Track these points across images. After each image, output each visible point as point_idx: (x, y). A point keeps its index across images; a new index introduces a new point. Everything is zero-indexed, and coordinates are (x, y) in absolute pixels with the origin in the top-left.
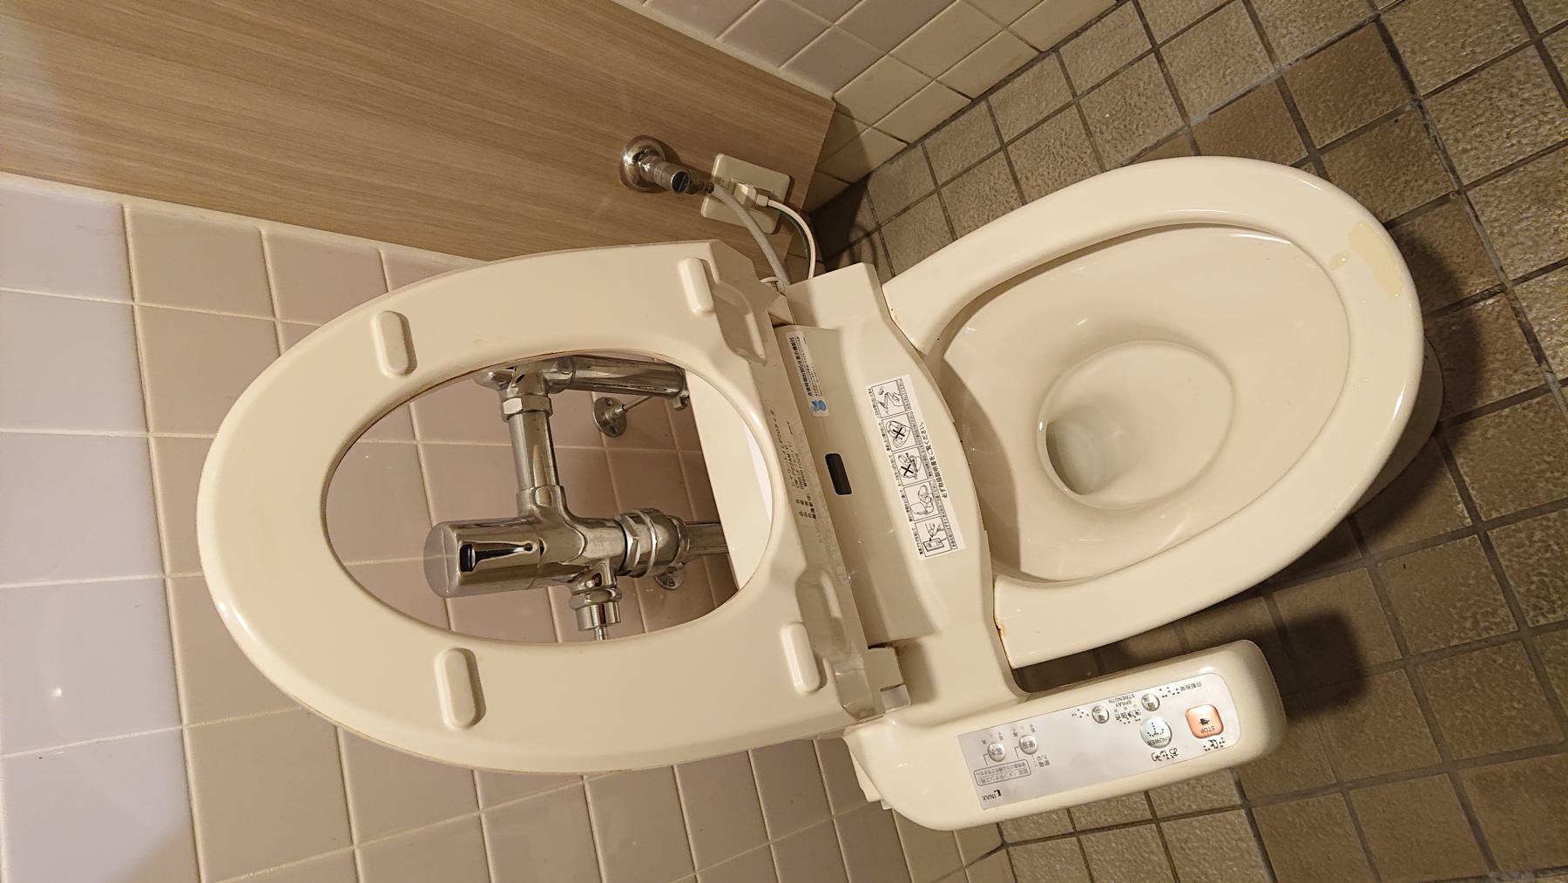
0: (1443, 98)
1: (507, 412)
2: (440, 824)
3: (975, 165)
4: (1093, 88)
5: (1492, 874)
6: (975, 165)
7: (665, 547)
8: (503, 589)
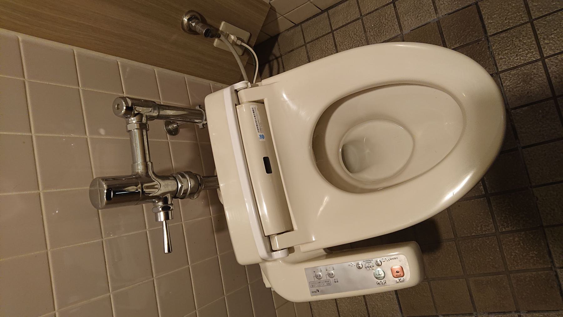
0: (496, 37)
1: (129, 129)
2: (93, 299)
3: (321, 37)
4: (368, 14)
5: (475, 313)
6: (321, 37)
7: (195, 186)
8: (124, 205)
